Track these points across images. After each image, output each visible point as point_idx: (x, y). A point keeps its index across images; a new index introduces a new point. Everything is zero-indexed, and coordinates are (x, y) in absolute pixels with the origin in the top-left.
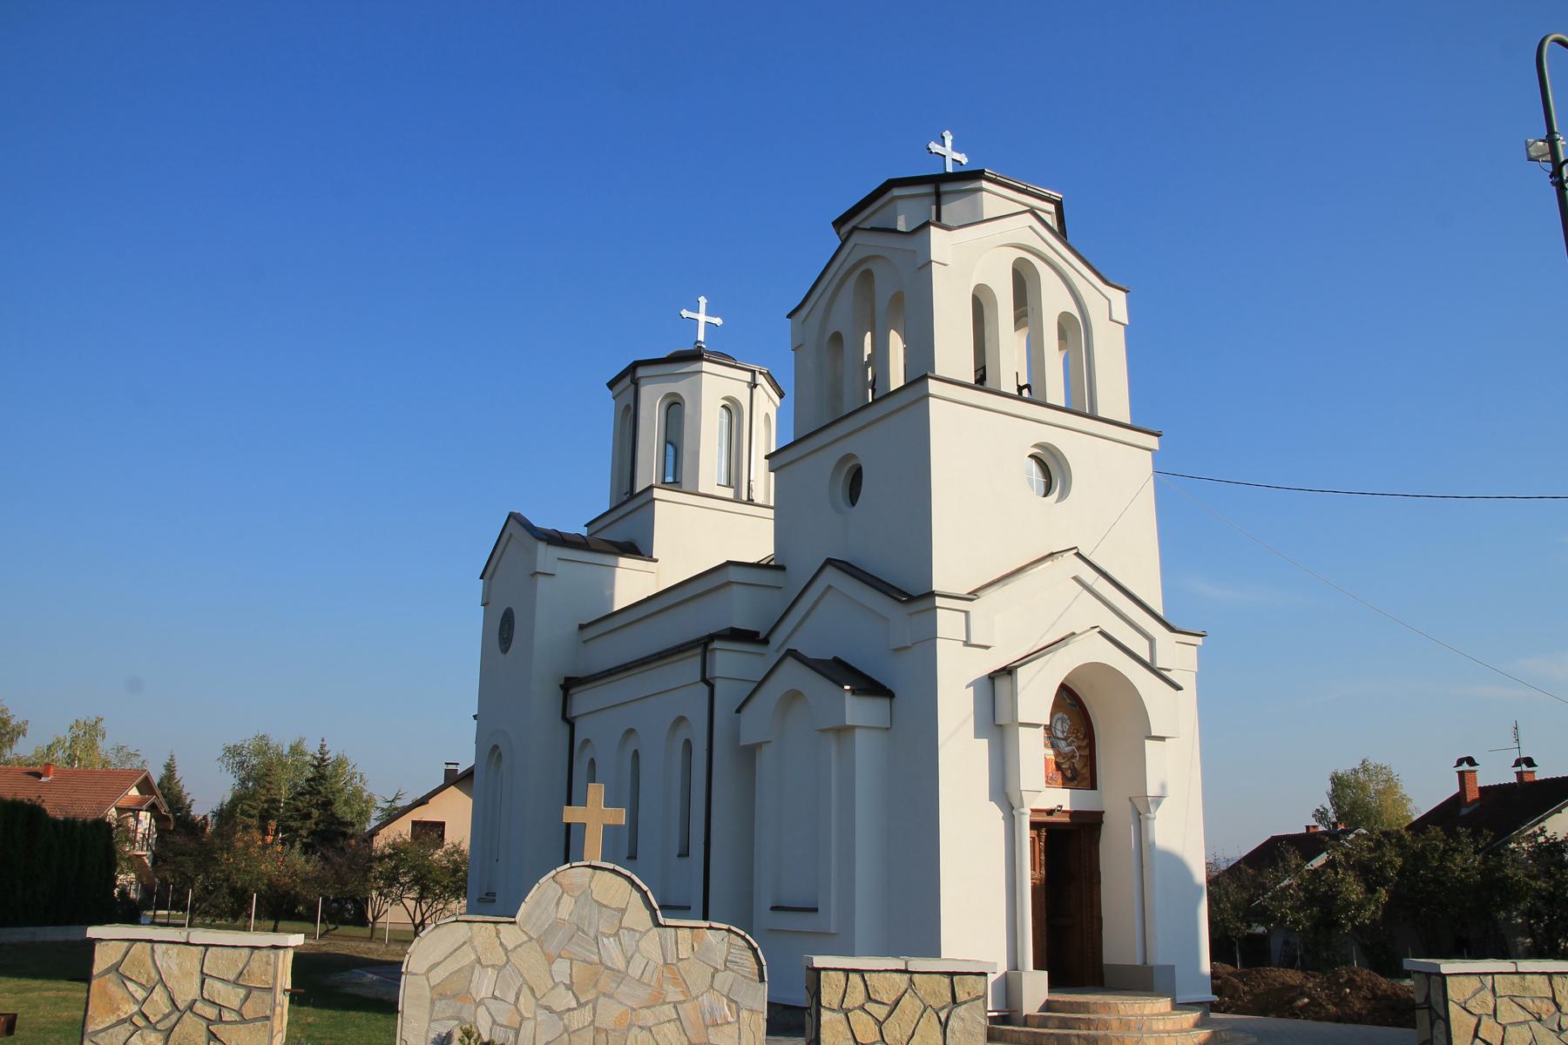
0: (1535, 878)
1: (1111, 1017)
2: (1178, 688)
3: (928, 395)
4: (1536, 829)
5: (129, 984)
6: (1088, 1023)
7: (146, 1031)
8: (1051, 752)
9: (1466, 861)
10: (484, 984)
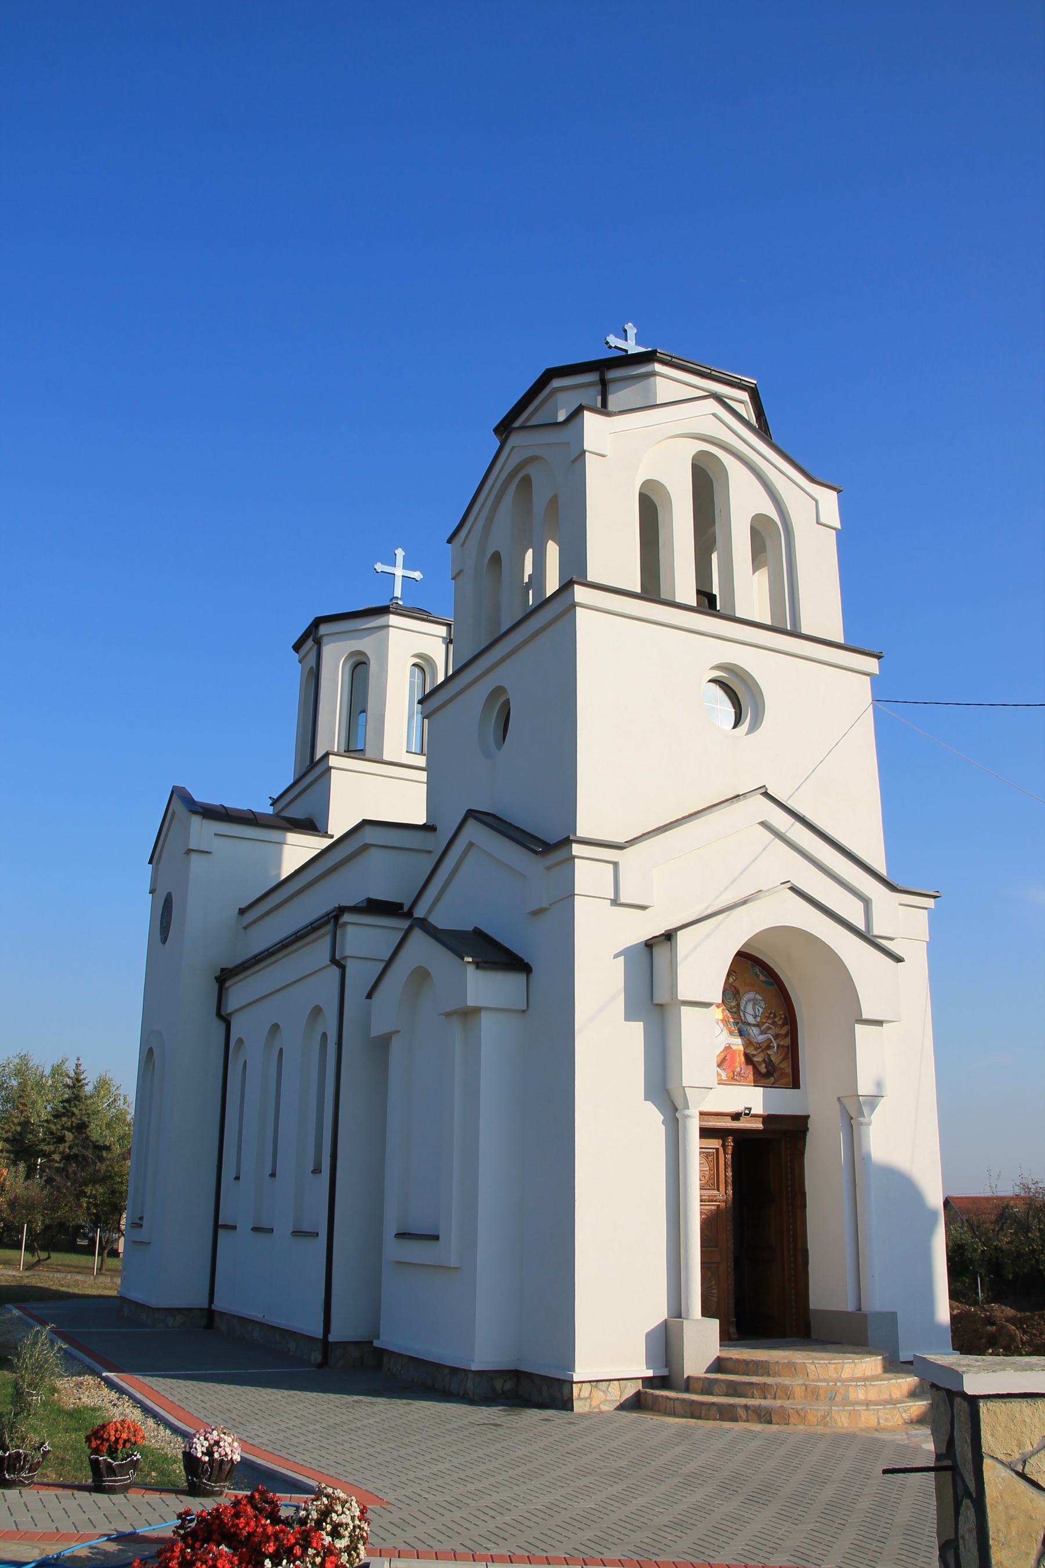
1: (794, 1383)
2: (899, 959)
3: (573, 605)
6: (764, 1390)
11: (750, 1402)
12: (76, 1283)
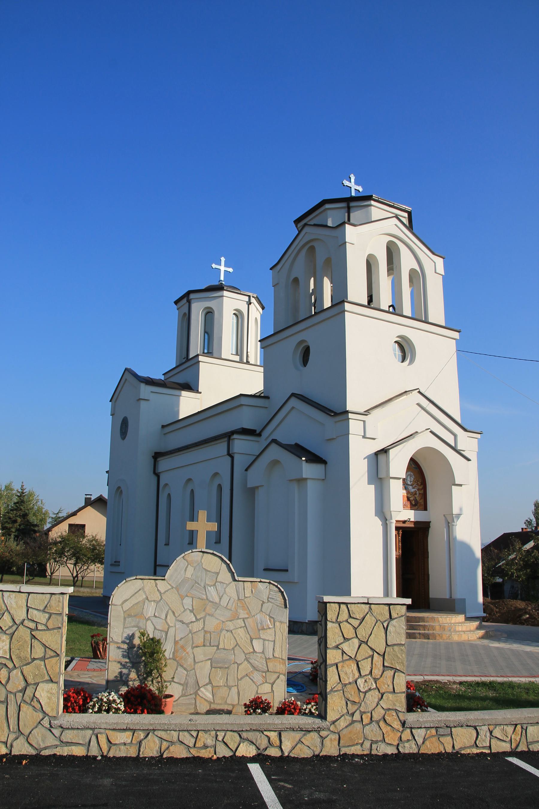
1: (436, 624)
2: (469, 460)
3: (344, 311)
6: (424, 627)
8: (405, 491)
10: (150, 610)
11: (418, 631)
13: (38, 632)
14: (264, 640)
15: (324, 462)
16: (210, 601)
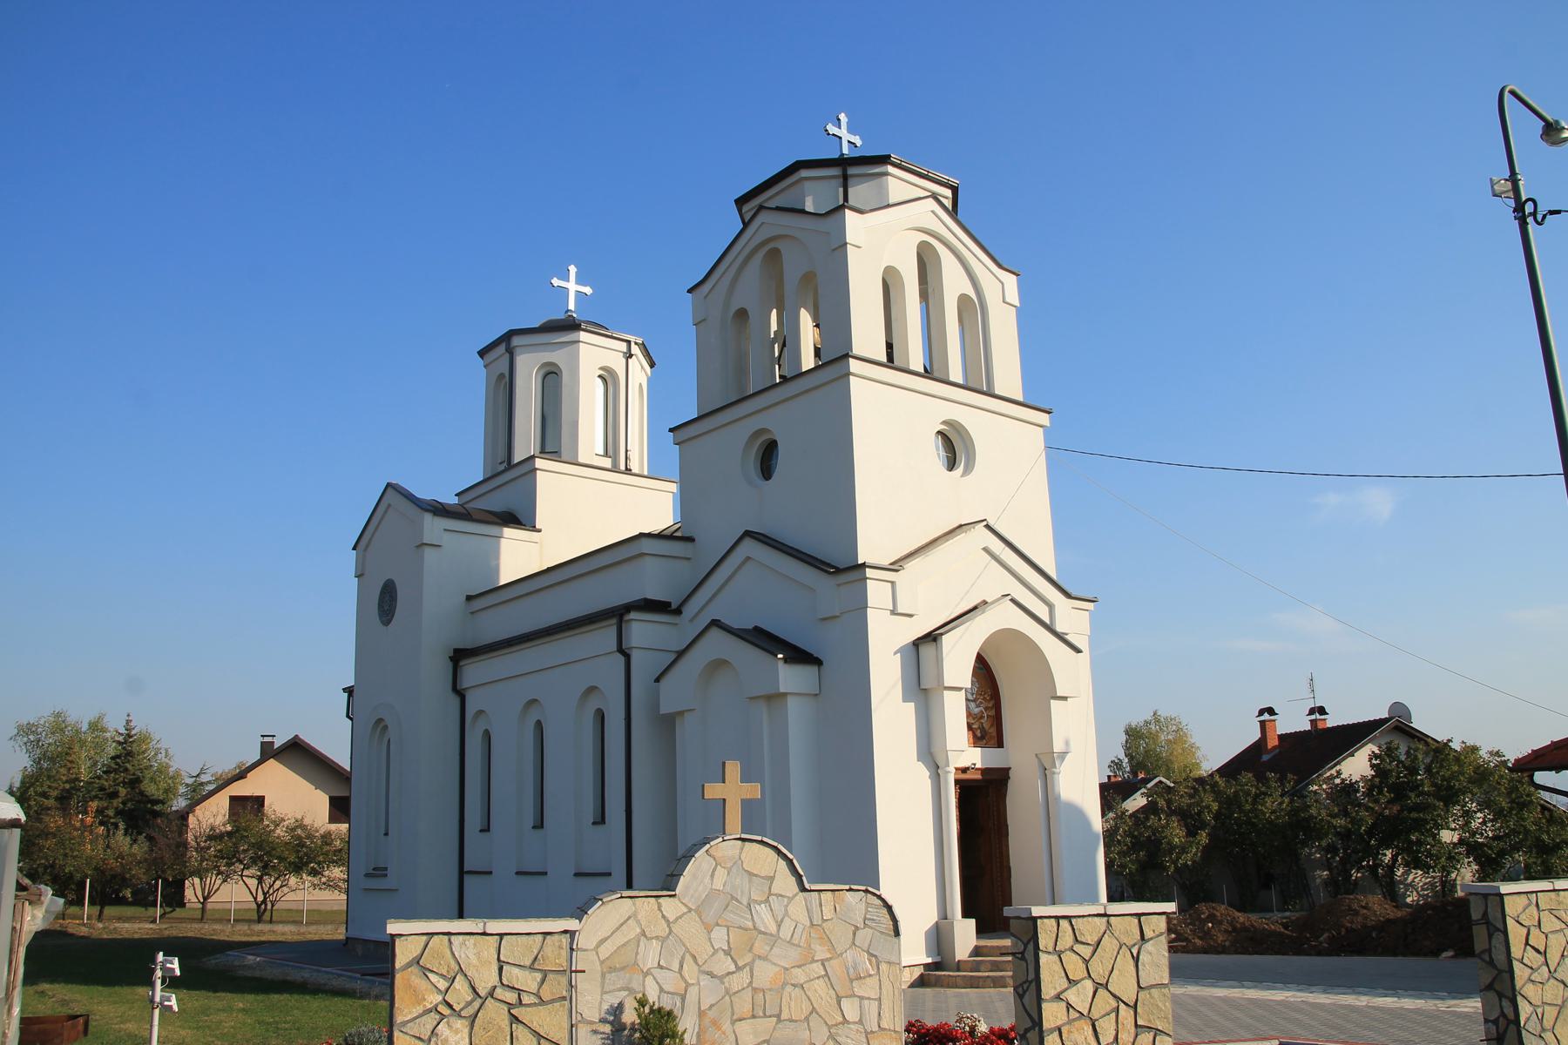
0: (1334, 816)
2: (1078, 651)
3: (848, 374)
4: (1333, 772)
5: (432, 976)
7: (452, 1019)
9: (1274, 804)
10: (650, 955)
12: (262, 932)
13: (523, 1009)
14: (862, 998)
15: (817, 662)
16: (761, 932)
